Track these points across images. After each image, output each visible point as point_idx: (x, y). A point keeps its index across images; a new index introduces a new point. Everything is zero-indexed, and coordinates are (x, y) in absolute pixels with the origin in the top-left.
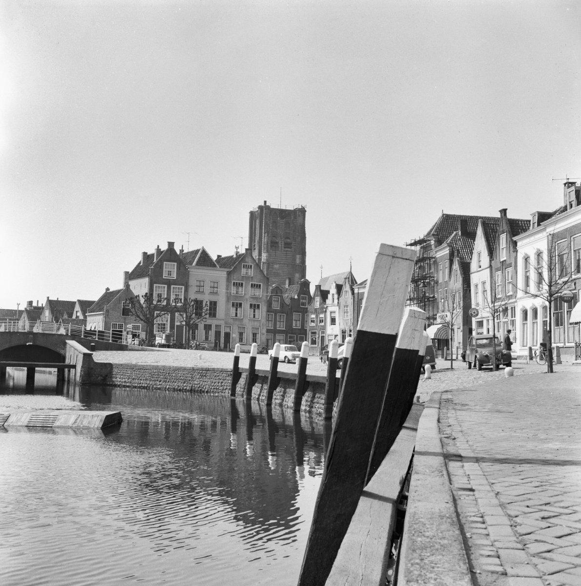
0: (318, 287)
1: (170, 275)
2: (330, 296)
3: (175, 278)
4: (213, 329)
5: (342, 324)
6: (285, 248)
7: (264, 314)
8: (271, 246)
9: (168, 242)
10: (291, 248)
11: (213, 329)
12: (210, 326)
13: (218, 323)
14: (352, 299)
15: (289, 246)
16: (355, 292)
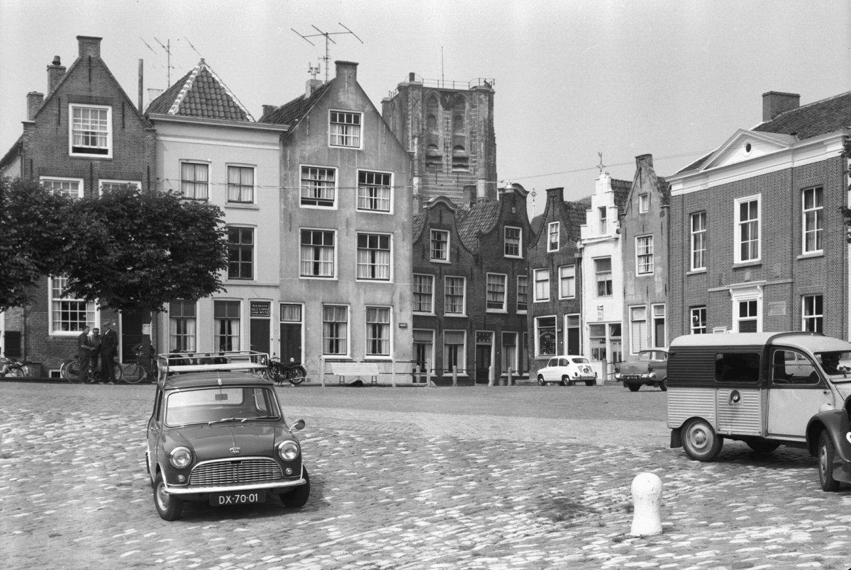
0: (555, 195)
1: (94, 143)
2: (592, 216)
3: (110, 156)
4: (245, 312)
5: (630, 291)
6: (454, 166)
7: (406, 266)
8: (427, 165)
9: (79, 38)
10: (466, 167)
11: (245, 312)
12: (235, 304)
13: (262, 295)
14: (662, 214)
15: (464, 164)
16: (673, 194)
